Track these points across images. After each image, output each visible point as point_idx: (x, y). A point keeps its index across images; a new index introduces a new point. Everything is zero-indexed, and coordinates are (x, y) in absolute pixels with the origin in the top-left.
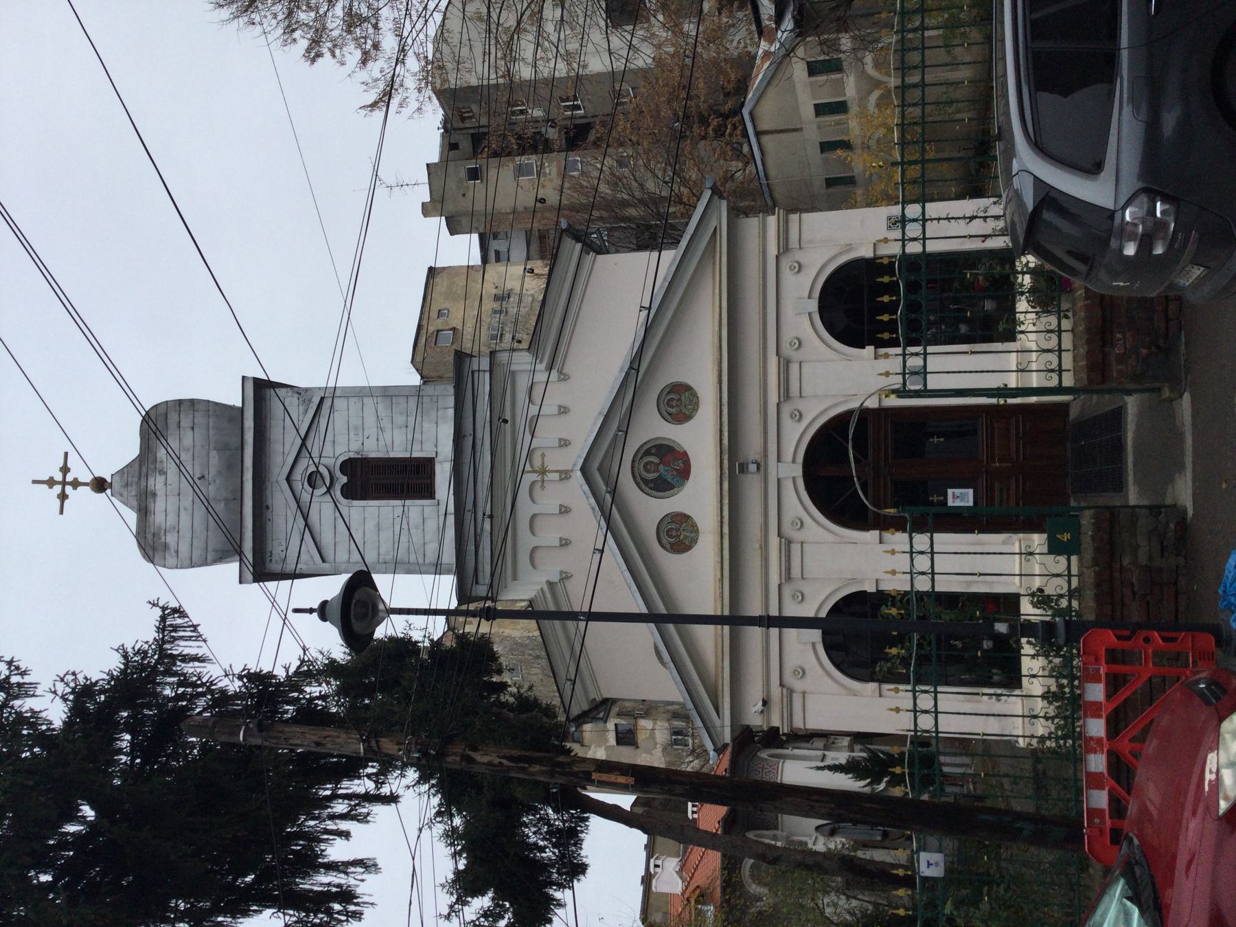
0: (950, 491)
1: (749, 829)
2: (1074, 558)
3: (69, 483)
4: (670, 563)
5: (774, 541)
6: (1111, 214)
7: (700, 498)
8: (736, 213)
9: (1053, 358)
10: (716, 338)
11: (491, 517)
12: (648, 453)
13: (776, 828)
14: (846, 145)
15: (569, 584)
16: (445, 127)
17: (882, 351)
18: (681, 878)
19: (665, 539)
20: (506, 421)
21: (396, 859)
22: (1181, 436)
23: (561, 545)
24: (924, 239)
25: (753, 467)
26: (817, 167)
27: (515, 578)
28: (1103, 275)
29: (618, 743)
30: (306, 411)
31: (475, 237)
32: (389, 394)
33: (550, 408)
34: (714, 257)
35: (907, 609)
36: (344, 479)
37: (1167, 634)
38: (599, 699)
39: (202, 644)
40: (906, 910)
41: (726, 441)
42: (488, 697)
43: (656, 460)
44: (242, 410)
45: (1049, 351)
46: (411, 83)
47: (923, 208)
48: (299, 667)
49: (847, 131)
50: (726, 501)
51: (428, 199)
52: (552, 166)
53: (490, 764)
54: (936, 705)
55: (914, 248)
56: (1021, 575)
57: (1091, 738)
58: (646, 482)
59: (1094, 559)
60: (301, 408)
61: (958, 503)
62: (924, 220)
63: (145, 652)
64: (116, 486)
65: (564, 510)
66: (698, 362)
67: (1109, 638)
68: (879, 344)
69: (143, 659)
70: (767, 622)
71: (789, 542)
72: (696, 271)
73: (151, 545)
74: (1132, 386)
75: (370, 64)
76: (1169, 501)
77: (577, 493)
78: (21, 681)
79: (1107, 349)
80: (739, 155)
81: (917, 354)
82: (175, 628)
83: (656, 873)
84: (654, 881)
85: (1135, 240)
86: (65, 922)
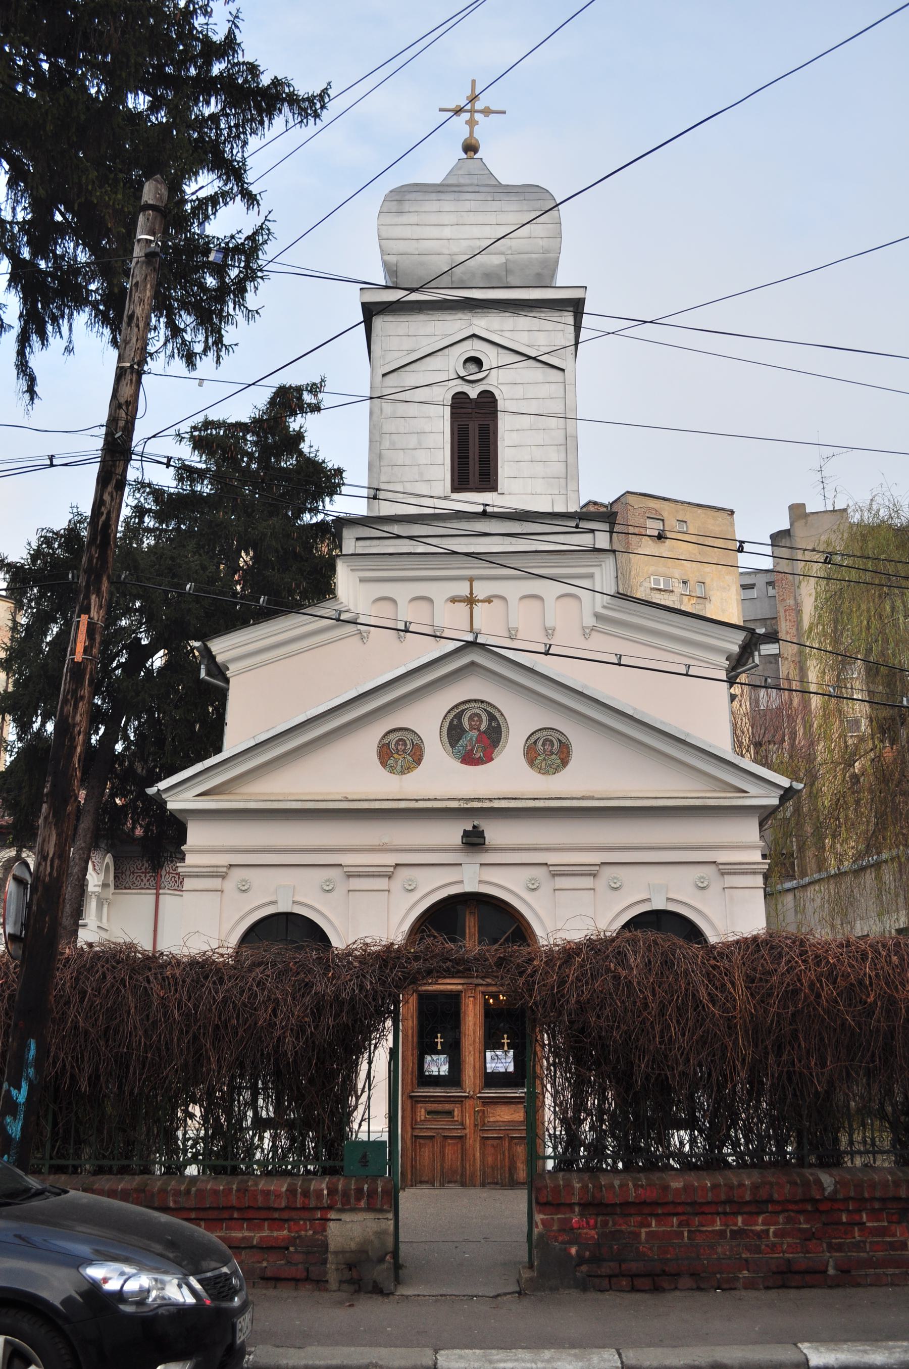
3: (472, 117)
4: (368, 740)
7: (442, 776)
8: (765, 816)
12: (492, 717)
13: (116, 887)
19: (394, 737)
27: (362, 580)
34: (715, 791)
41: (496, 804)
43: (483, 727)
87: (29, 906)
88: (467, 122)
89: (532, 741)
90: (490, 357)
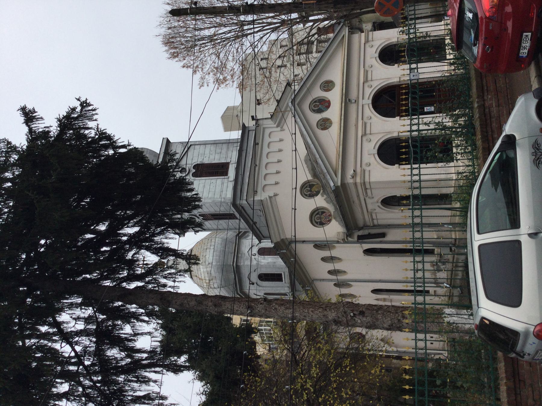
7: (334, 113)
12: (315, 102)
15: (277, 197)
19: (320, 127)
24: (420, 175)
36: (194, 171)
40: (409, 366)
44: (159, 154)
58: (306, 195)
62: (421, 188)
81: (419, 231)
89: (316, 225)
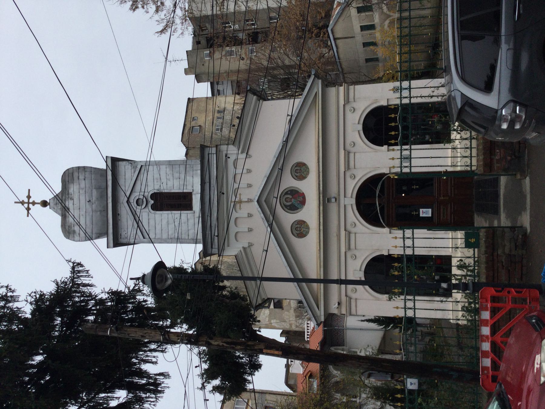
0: (421, 210)
1: (332, 346)
2: (476, 250)
3: (31, 203)
4: (296, 242)
5: (343, 233)
6: (496, 111)
7: (310, 213)
9: (468, 142)
10: (317, 143)
11: (218, 236)
12: (286, 193)
13: (344, 345)
14: (374, 44)
16: (194, 34)
17: (391, 148)
18: (302, 366)
19: (295, 232)
20: (223, 194)
21: (178, 372)
22: (525, 197)
23: (249, 231)
25: (333, 200)
26: (362, 54)
27: (228, 246)
28: (492, 134)
29: (275, 307)
30: (135, 172)
31: (209, 83)
32: (171, 164)
33: (243, 184)
34: (316, 105)
35: (402, 272)
36: (152, 202)
37: (518, 290)
38: (266, 298)
39: (90, 279)
40: (398, 272)
41: (321, 189)
42: (218, 292)
43: (291, 197)
45: (466, 157)
46: (178, 21)
47: (410, 83)
48: (134, 287)
49: (375, 38)
50: (322, 215)
51: (187, 67)
52: (243, 51)
53: (218, 345)
54: (414, 306)
55: (405, 101)
56: (452, 238)
57: (484, 335)
58: (286, 206)
59: (485, 251)
60: (133, 170)
61: (424, 215)
63: (66, 283)
64: (52, 204)
65: (250, 215)
66: (308, 153)
67: (491, 291)
68: (390, 145)
69: (65, 285)
70: (340, 282)
71: (350, 233)
72: (308, 111)
73: (68, 231)
74: (504, 173)
75: (160, 13)
76: (519, 224)
77: (254, 208)
78: (12, 295)
79: (493, 157)
80: (326, 46)
81: (406, 150)
82: (79, 272)
83: (291, 364)
84: (291, 368)
85: (507, 122)
86: (33, 407)
87: (379, 372)
88: (33, 205)
90: (136, 195)
